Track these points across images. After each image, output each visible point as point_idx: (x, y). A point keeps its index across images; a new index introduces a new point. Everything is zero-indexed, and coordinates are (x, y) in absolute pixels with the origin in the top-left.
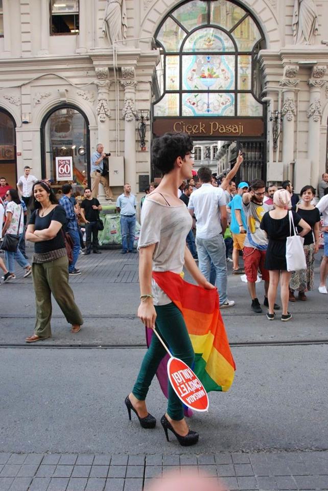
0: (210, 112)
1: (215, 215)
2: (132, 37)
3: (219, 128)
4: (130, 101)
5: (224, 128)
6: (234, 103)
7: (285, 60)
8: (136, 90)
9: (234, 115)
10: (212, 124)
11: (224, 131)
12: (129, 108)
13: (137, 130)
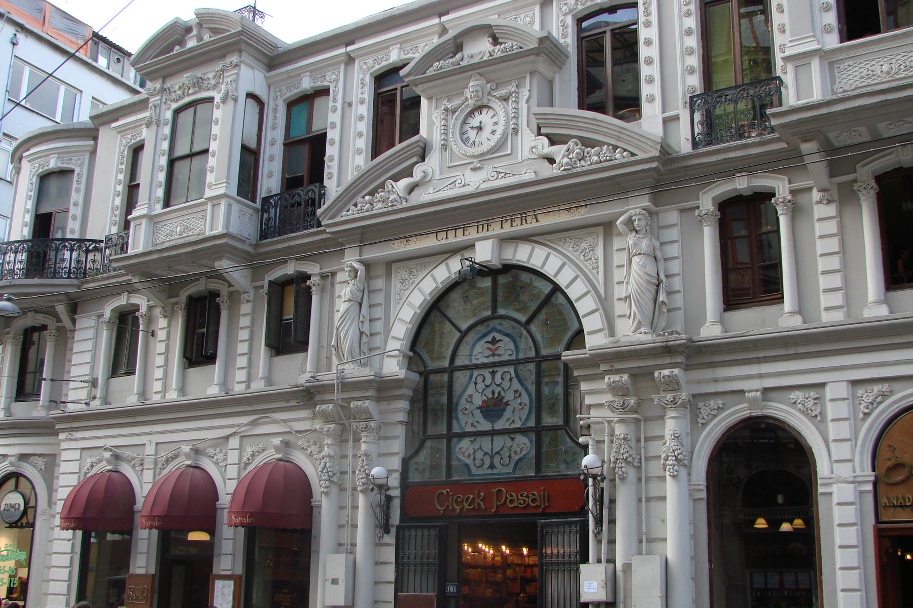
3: (507, 498)
13: (380, 506)
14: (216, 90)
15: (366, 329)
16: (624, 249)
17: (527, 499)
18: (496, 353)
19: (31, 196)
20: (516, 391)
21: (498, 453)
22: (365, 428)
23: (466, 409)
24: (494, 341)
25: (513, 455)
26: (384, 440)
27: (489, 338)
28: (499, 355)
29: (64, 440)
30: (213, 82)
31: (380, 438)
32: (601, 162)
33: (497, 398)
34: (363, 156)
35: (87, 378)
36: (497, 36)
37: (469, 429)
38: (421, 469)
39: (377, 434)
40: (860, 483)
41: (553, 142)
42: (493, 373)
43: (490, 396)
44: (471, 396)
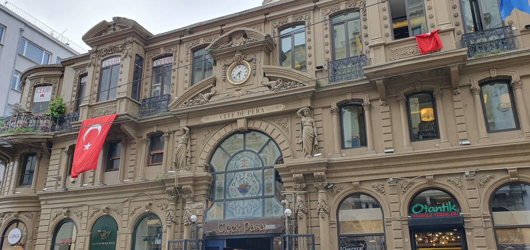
3: (250, 227)
5: (254, 227)
7: (292, 171)
10: (245, 224)
11: (254, 229)
14: (122, 52)
15: (189, 155)
16: (300, 124)
17: (259, 227)
19: (30, 95)
20: (254, 181)
21: (246, 207)
24: (244, 161)
25: (252, 208)
27: (242, 159)
29: (43, 205)
30: (120, 49)
32: (291, 88)
34: (188, 83)
35: (56, 176)
36: (247, 35)
37: (233, 197)
40: (403, 221)
41: (270, 80)
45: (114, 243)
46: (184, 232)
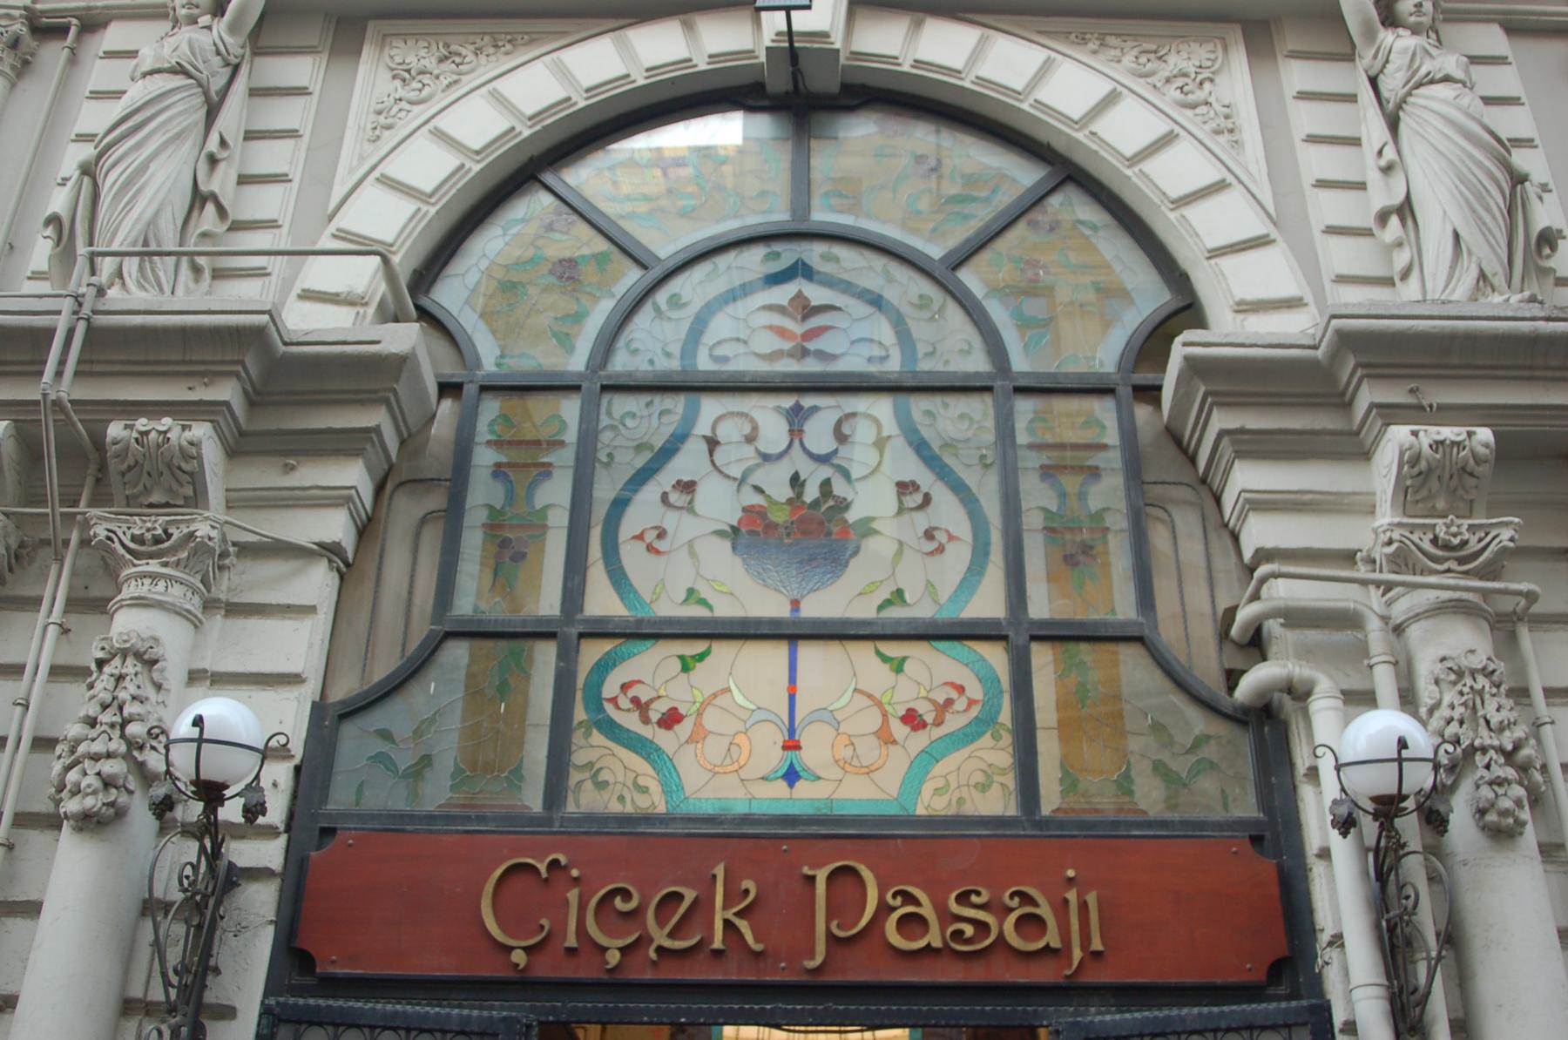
0: (803, 789)
1: (685, 36)
2: (271, 224)
3: (884, 909)
4: (131, 667)
5: (927, 910)
6: (1005, 716)
8: (209, 605)
9: (1012, 811)
10: (822, 876)
11: (934, 938)
12: (107, 717)
18: (811, 346)
20: (904, 487)
22: (157, 541)
23: (662, 534)
26: (733, 290)
28: (822, 355)
31: (209, 605)
33: (816, 504)
37: (669, 607)
38: (404, 761)
39: (205, 581)
42: (797, 419)
43: (783, 492)
44: (688, 487)
45: (272, 1001)
46: (32, 909)
